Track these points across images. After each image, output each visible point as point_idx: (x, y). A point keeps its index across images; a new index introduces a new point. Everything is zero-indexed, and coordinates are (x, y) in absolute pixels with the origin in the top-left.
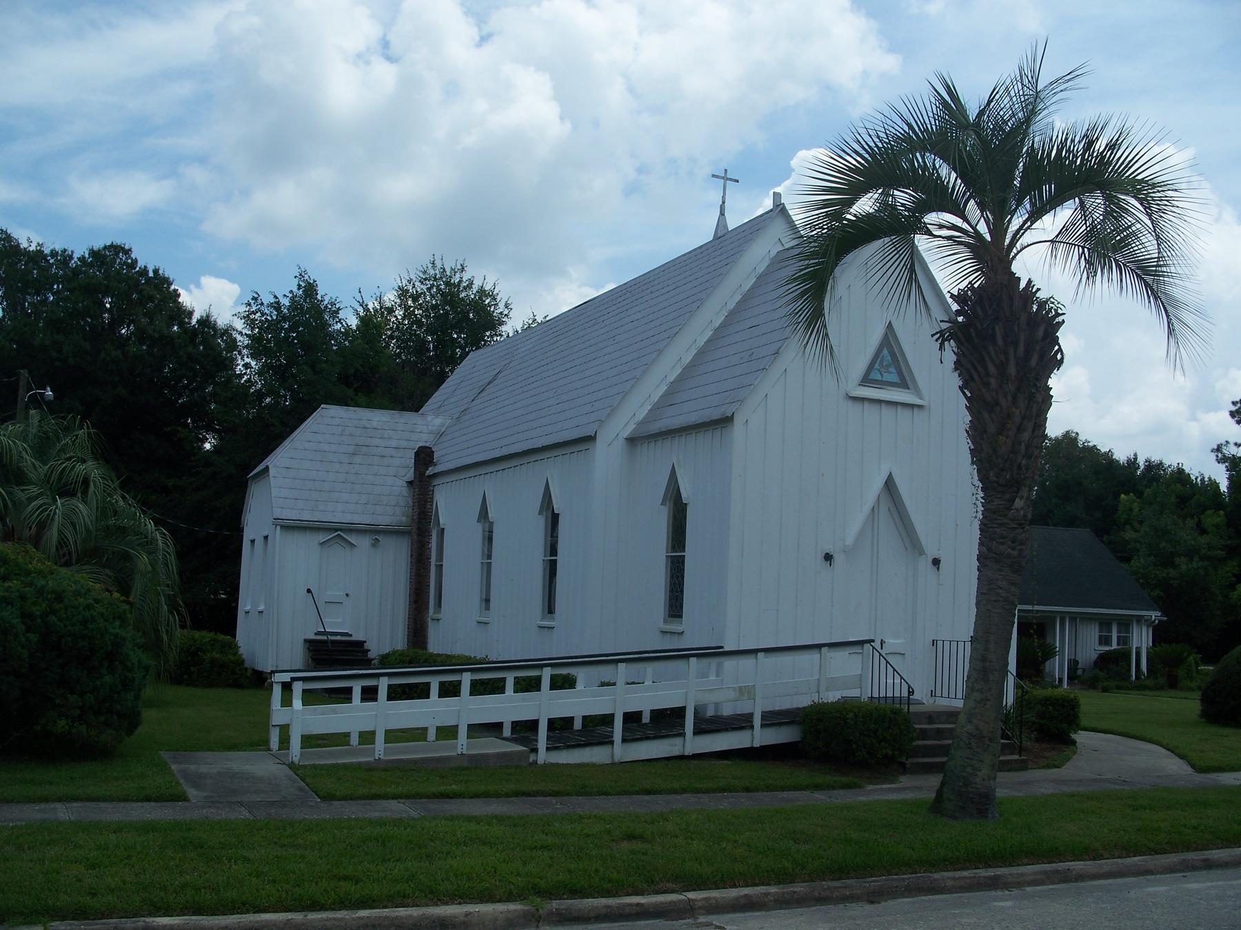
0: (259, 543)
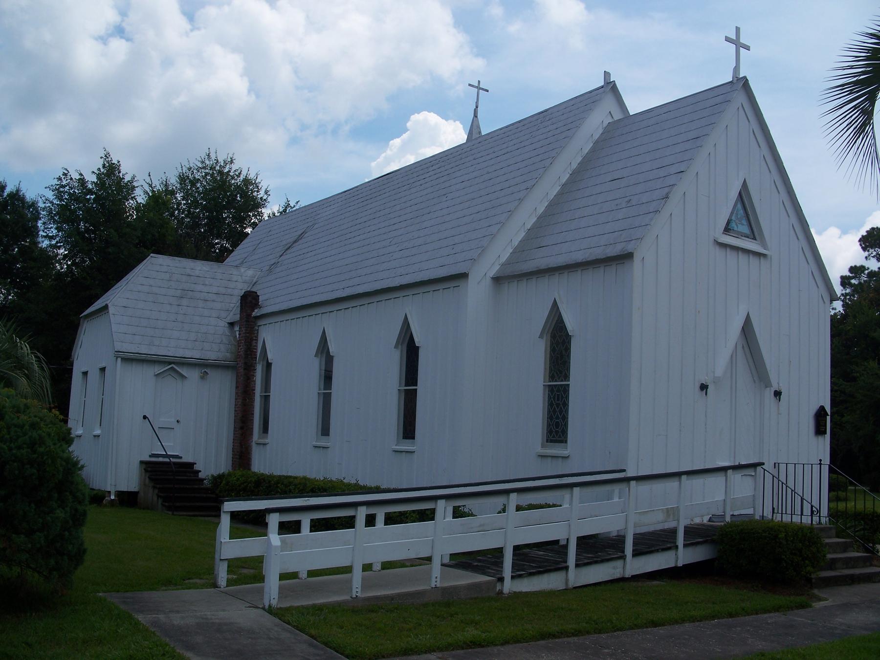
0: (94, 376)
